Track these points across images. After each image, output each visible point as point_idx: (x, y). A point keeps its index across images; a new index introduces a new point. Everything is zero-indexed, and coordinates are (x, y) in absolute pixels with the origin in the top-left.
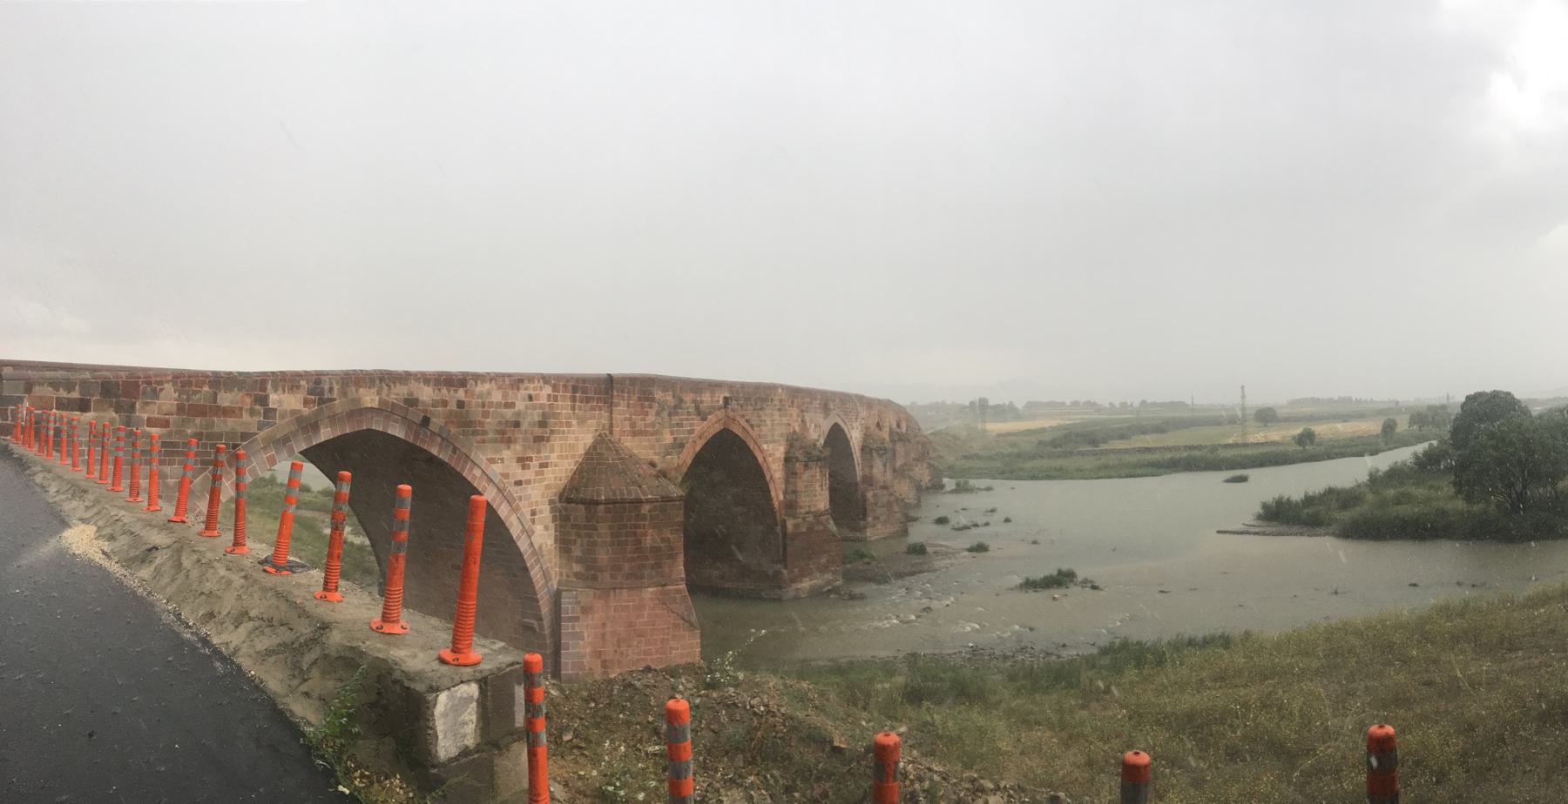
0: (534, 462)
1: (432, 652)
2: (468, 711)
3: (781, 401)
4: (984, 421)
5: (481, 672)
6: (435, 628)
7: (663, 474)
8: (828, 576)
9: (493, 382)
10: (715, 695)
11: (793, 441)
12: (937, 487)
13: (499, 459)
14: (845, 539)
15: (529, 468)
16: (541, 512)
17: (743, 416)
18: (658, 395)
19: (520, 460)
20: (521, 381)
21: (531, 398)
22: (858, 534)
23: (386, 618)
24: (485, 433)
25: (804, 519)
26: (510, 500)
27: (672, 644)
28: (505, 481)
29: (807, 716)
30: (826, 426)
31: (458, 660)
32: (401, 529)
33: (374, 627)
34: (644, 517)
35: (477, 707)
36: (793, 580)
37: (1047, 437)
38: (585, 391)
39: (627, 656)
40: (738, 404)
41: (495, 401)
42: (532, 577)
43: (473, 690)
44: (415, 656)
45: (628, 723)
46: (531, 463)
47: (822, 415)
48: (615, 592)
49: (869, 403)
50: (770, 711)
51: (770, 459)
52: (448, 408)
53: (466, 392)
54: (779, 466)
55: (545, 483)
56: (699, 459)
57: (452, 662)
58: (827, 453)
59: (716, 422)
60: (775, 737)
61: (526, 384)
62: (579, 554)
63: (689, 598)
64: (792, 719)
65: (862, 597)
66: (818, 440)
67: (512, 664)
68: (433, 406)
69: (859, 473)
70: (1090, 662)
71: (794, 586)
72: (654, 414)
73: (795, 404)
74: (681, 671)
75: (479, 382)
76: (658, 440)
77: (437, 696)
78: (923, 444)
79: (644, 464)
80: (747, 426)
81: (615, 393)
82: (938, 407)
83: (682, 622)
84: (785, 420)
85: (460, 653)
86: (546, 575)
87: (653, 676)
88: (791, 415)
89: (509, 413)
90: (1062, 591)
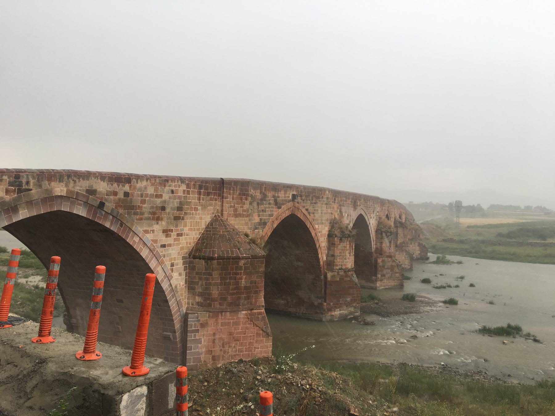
0: (174, 233)
1: (118, 369)
2: (140, 403)
3: (327, 198)
4: (458, 217)
5: (149, 379)
6: (119, 353)
7: (253, 241)
8: (352, 309)
9: (149, 180)
10: (279, 377)
11: (333, 224)
12: (424, 259)
13: (151, 231)
14: (363, 287)
15: (171, 237)
16: (177, 265)
17: (304, 207)
18: (252, 192)
19: (164, 231)
20: (167, 181)
21: (172, 192)
22: (371, 285)
23: (86, 351)
24: (142, 214)
25: (338, 272)
26: (157, 257)
27: (256, 345)
28: (154, 245)
29: (334, 393)
30: (354, 215)
31: (135, 373)
32: (98, 294)
33: (78, 357)
34: (241, 268)
35: (146, 400)
36: (330, 310)
37: (505, 231)
38: (207, 188)
39: (228, 353)
40: (301, 199)
41: (149, 193)
42: (170, 306)
43: (144, 390)
44: (107, 374)
45: (228, 394)
46: (172, 233)
47: (353, 209)
48: (222, 315)
49: (382, 202)
50: (312, 388)
51: (319, 234)
52: (118, 196)
53: (130, 187)
54: (324, 239)
55: (181, 246)
56: (275, 232)
57: (131, 375)
58: (354, 232)
59: (287, 210)
60: (315, 404)
61: (170, 183)
62: (200, 290)
63: (266, 318)
64: (326, 394)
65: (372, 324)
66: (349, 224)
67: (168, 372)
68: (107, 195)
69: (374, 246)
70: (529, 390)
71: (330, 313)
72: (248, 204)
73: (336, 201)
74: (260, 362)
75: (139, 180)
76: (250, 220)
77: (122, 396)
78: (416, 230)
79: (242, 235)
80: (306, 213)
81: (225, 190)
82: (426, 205)
83: (261, 332)
84: (329, 211)
85: (136, 369)
86: (179, 304)
87: (244, 365)
88: (333, 208)
89: (158, 201)
90: (511, 339)
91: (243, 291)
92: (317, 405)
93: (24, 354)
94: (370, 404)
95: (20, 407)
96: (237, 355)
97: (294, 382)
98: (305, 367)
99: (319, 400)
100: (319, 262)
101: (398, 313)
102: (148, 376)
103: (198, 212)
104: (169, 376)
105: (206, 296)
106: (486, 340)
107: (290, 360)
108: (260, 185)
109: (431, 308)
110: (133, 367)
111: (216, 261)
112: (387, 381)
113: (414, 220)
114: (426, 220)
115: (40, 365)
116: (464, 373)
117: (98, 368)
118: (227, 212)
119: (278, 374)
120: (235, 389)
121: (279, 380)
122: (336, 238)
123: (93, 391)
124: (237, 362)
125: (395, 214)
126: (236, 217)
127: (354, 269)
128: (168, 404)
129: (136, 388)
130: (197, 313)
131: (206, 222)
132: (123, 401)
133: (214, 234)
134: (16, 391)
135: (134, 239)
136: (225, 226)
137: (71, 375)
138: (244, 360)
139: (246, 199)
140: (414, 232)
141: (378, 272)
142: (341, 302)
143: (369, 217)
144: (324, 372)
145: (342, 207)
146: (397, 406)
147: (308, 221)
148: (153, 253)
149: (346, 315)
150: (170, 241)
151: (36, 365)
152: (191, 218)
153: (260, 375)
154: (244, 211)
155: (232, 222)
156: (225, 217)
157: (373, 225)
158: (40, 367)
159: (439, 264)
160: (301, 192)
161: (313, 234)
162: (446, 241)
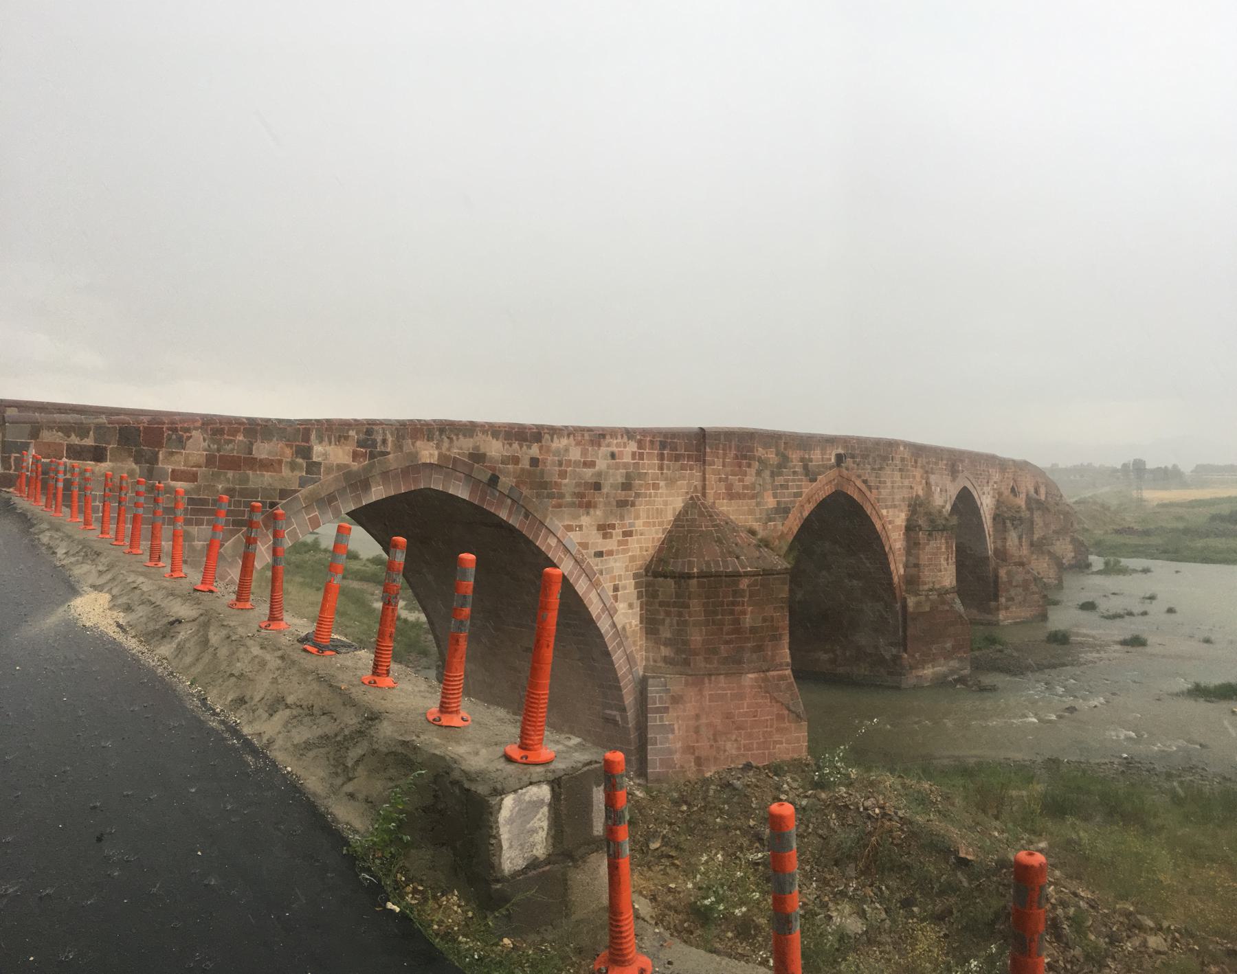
0: (617, 530)
1: (497, 748)
2: (538, 817)
3: (903, 459)
5: (554, 771)
7: (765, 543)
8: (954, 664)
10: (823, 796)
11: (916, 507)
12: (1082, 566)
13: (576, 526)
14: (973, 622)
15: (611, 537)
16: (625, 588)
17: (859, 476)
18: (760, 452)
20: (603, 436)
21: (613, 456)
22: (989, 617)
23: (444, 708)
24: (561, 496)
25: (927, 596)
27: (776, 737)
30: (953, 491)
31: (527, 757)
35: (549, 811)
37: (1225, 510)
39: (725, 751)
40: (854, 462)
43: (544, 792)
44: (477, 754)
45: (726, 829)
48: (710, 680)
49: (1002, 465)
51: (890, 527)
53: (541, 448)
54: (899, 535)
55: (630, 554)
56: (806, 525)
58: (954, 521)
61: (608, 440)
62: (669, 635)
63: (795, 685)
64: (911, 823)
65: (993, 689)
66: (943, 507)
67: (590, 763)
69: (990, 546)
72: (754, 475)
73: (919, 464)
74: (786, 768)
75: (555, 436)
78: (1067, 514)
80: (863, 488)
81: (708, 450)
82: (1080, 470)
84: (906, 483)
85: (529, 750)
86: (630, 659)
88: (914, 477)
89: (588, 473)
91: (748, 635)
92: (897, 845)
93: (349, 701)
94: (996, 837)
95: (335, 791)
96: (743, 755)
97: (851, 804)
98: (872, 774)
99: (900, 836)
100: (892, 579)
101: (1040, 668)
102: (552, 767)
103: (660, 491)
104: (592, 770)
105: (679, 643)
106: (1201, 707)
107: (841, 760)
108: (771, 438)
109: (1097, 655)
110: (523, 746)
111: (694, 581)
112: (1024, 793)
113: (1061, 496)
114: (1083, 496)
115: (370, 722)
116: (1165, 770)
117: (462, 743)
118: (712, 489)
119: (819, 790)
120: (739, 819)
121: (823, 800)
122: (921, 533)
123: (451, 782)
124: (742, 769)
125: (1027, 485)
126: (731, 499)
127: (956, 589)
128: (591, 827)
129: (528, 785)
130: (664, 678)
131: (674, 509)
132: (503, 808)
133: (690, 532)
134: (332, 762)
135: (548, 540)
136: (711, 516)
137: (415, 748)
138: (754, 764)
139: (749, 466)
140: (1062, 517)
141: (1000, 593)
142: (934, 651)
143: (980, 493)
144: (908, 781)
145: (930, 475)
146: (1046, 839)
147: (868, 504)
148: (581, 567)
149: (945, 676)
150: (611, 544)
151: (364, 722)
152: (648, 503)
153: (786, 793)
154: (745, 487)
155: (724, 508)
156: (710, 499)
157: (987, 506)
158: (370, 726)
159: (1110, 574)
160: (853, 448)
161: (878, 526)
162: (1120, 533)
